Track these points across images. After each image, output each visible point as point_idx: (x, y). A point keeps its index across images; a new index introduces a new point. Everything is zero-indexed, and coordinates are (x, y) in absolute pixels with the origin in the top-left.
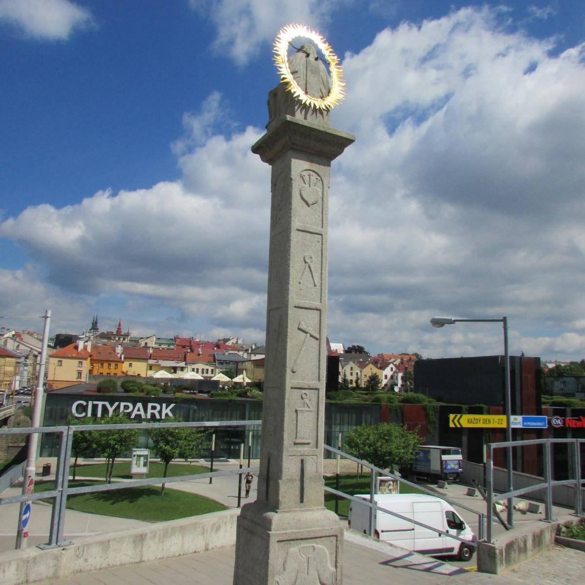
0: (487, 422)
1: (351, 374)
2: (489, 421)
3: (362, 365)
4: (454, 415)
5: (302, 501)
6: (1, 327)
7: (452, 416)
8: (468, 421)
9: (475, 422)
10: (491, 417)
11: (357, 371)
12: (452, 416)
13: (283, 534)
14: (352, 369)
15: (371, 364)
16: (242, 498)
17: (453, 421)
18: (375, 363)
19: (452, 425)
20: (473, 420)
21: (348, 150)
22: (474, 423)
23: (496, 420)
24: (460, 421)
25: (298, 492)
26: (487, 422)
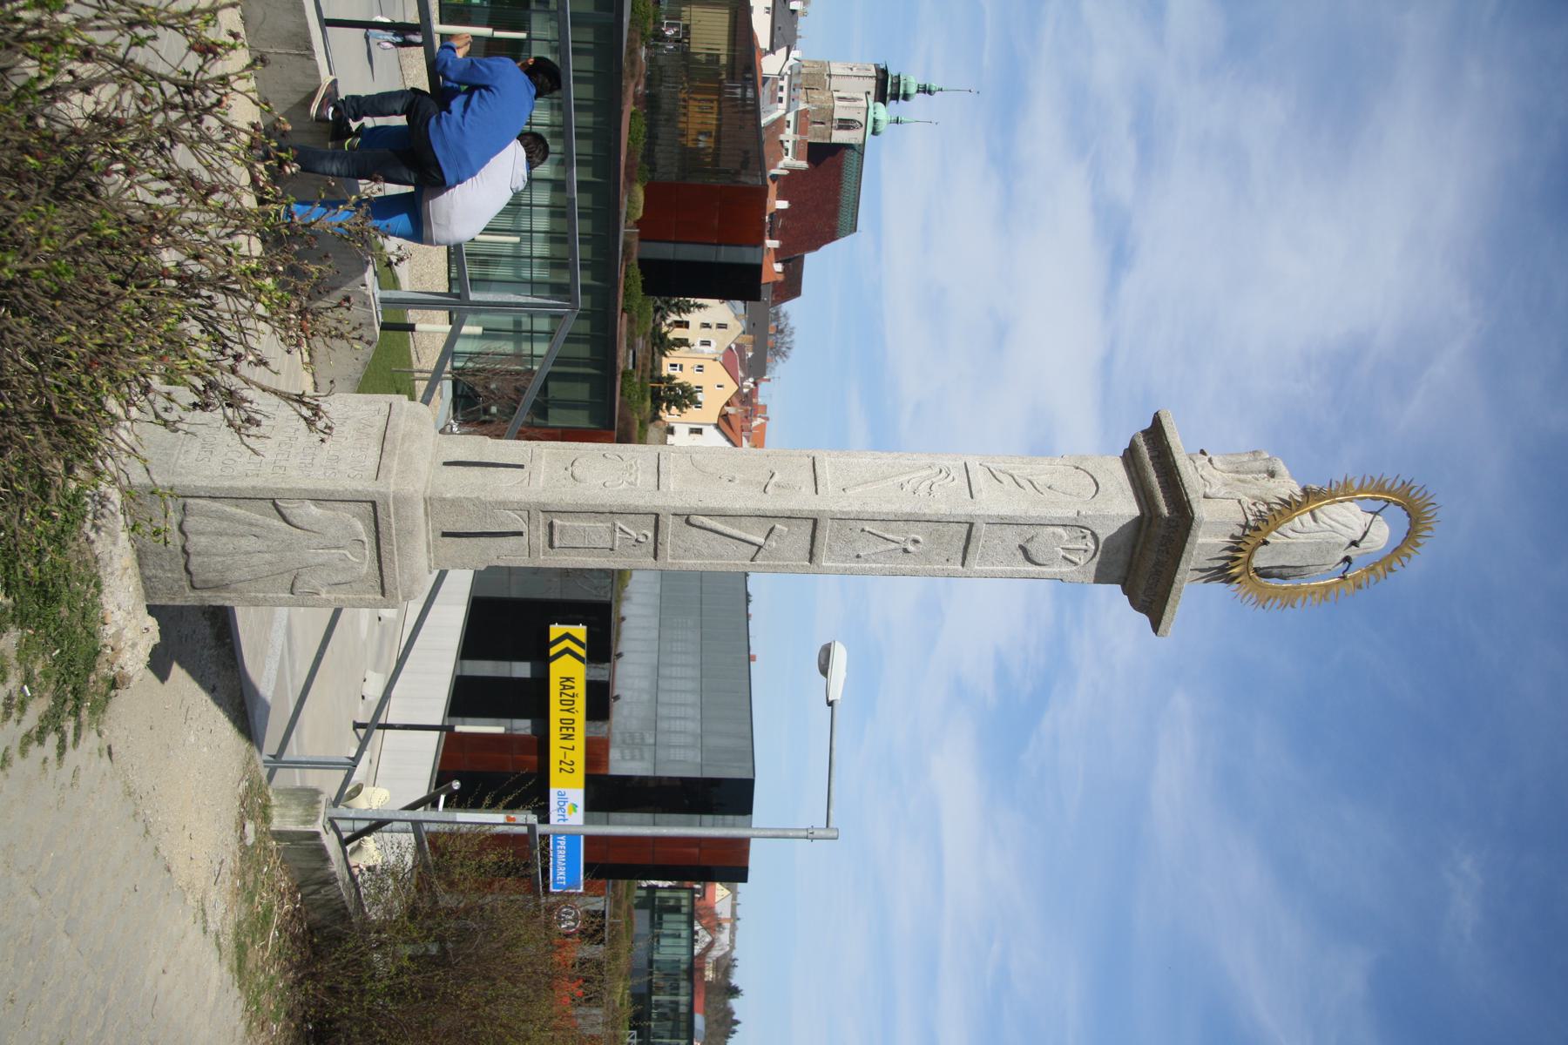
0: (564, 731)
1: (706, 325)
2: (567, 737)
3: (730, 360)
4: (583, 638)
5: (445, 534)
6: (630, 1039)
7: (580, 631)
8: (568, 679)
9: (564, 697)
10: (579, 742)
11: (713, 344)
12: (580, 631)
13: (389, 511)
14: (721, 326)
15: (736, 388)
16: (511, 671)
17: (567, 636)
18: (745, 400)
19: (556, 630)
20: (570, 692)
21: (1143, 620)
22: (561, 694)
23: (571, 756)
24: (567, 656)
25: (459, 528)
26: (564, 731)
